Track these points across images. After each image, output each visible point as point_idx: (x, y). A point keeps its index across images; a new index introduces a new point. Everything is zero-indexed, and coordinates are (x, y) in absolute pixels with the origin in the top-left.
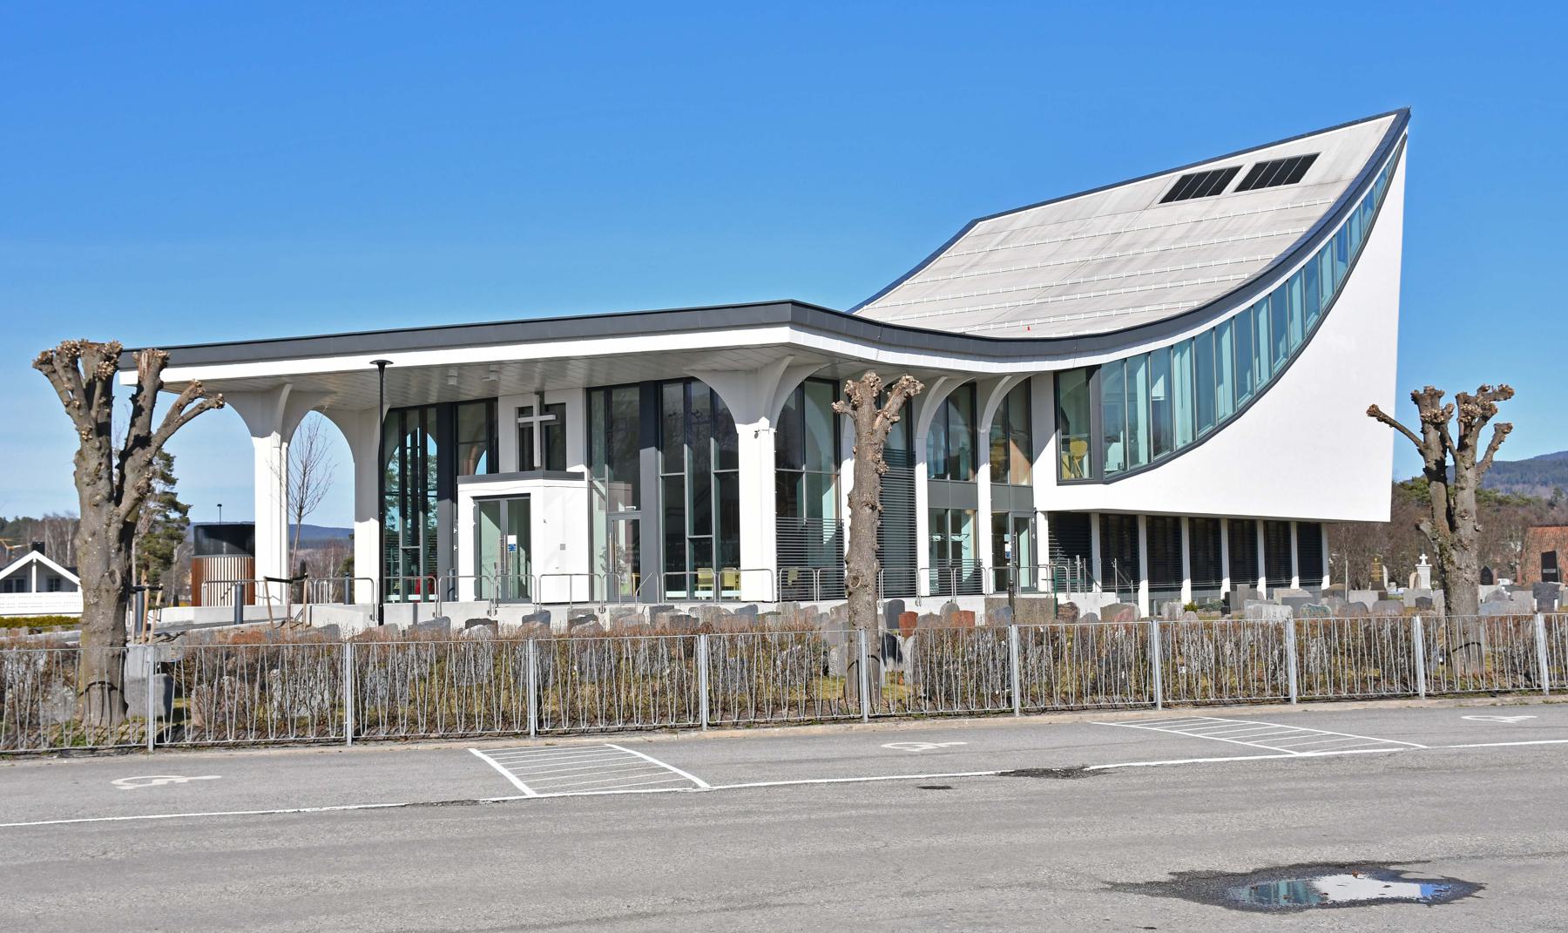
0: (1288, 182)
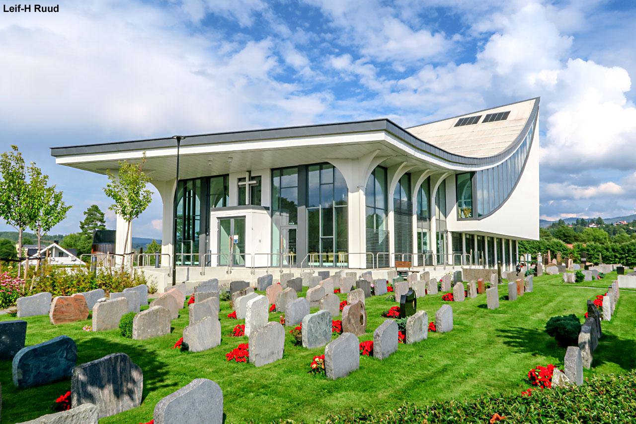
0: (496, 120)
